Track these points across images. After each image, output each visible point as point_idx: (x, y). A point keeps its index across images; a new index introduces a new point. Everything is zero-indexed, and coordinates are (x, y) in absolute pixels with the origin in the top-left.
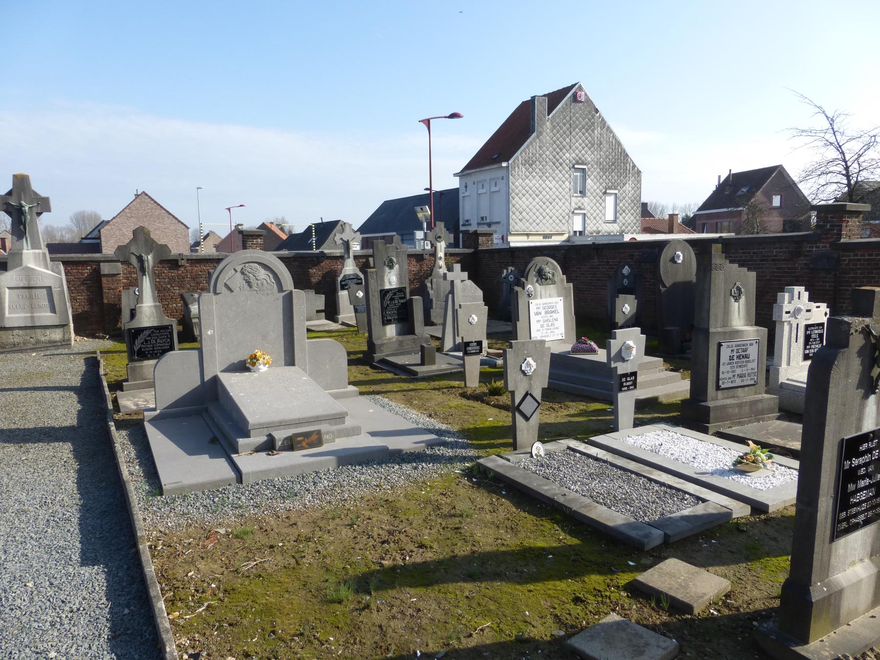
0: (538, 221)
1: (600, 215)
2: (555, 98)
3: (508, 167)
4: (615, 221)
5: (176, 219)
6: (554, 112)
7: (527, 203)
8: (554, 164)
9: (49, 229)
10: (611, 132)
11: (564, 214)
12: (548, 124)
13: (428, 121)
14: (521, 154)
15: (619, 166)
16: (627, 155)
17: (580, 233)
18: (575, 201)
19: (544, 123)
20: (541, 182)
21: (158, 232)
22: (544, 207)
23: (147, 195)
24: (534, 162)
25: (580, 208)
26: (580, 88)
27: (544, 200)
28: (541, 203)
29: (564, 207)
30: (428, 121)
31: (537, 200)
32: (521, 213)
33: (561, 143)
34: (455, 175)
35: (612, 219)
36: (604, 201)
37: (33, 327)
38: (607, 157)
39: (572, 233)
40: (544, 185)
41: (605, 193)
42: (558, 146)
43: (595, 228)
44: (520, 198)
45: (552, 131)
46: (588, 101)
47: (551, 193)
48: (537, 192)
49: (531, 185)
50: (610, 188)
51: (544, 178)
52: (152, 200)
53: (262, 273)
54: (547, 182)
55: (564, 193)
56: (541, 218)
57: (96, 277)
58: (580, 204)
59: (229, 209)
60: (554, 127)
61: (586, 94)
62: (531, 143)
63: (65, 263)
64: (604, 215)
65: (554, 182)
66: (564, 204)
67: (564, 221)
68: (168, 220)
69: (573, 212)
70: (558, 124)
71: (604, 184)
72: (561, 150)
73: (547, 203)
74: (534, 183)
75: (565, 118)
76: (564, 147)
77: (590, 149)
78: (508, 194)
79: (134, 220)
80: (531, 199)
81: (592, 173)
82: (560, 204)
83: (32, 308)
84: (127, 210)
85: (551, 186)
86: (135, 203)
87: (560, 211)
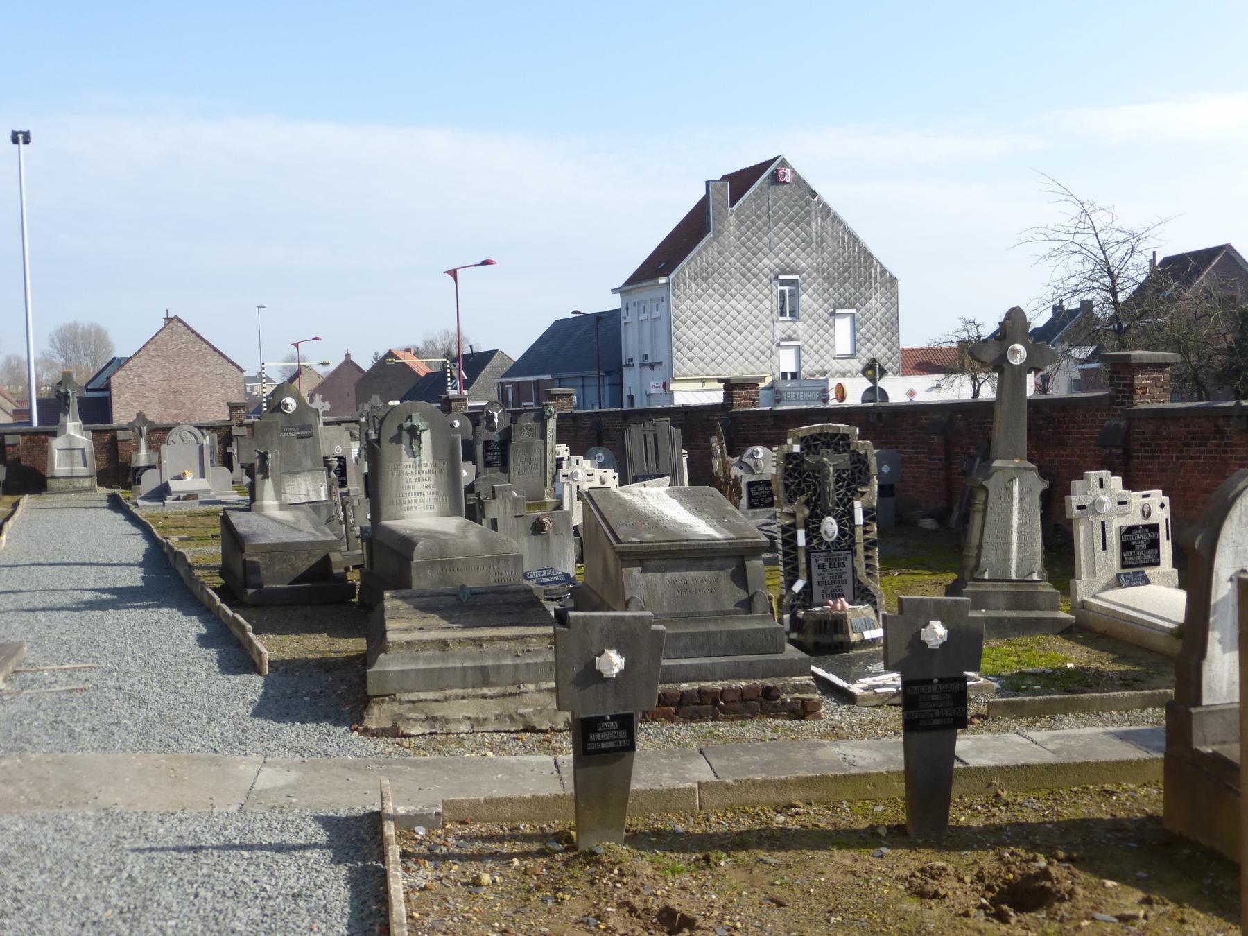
0: (719, 359)
1: (827, 347)
2: (740, 182)
3: (668, 284)
4: (853, 356)
5: (225, 357)
6: (741, 201)
7: (701, 333)
8: (744, 275)
9: (14, 363)
10: (840, 222)
11: (763, 348)
12: (732, 219)
13: (455, 271)
14: (688, 264)
15: (857, 275)
16: (870, 255)
17: (794, 375)
18: (783, 326)
19: (725, 219)
20: (722, 302)
21: (196, 379)
22: (729, 338)
23: (180, 321)
24: (710, 275)
25: (790, 338)
26: (784, 164)
27: (729, 328)
28: (724, 334)
29: (762, 338)
30: (455, 271)
31: (717, 328)
32: (690, 349)
33: (755, 244)
34: (614, 291)
35: (848, 351)
36: (833, 326)
37: (72, 477)
38: (835, 260)
39: (778, 376)
40: (728, 307)
41: (833, 314)
42: (749, 249)
43: (817, 367)
44: (689, 328)
45: (738, 228)
46: (798, 181)
47: (740, 318)
48: (717, 317)
49: (706, 307)
50: (842, 306)
51: (728, 296)
52: (189, 328)
53: (189, 435)
54: (733, 302)
55: (761, 317)
56: (724, 354)
57: (114, 441)
58: (789, 332)
59: (453, 273)
60: (742, 223)
61: (793, 172)
62: (705, 248)
63: (93, 431)
64: (834, 347)
65: (744, 302)
66: (762, 333)
67: (763, 358)
68: (212, 359)
69: (778, 345)
70: (748, 218)
71: (831, 301)
72: (755, 254)
73: (735, 333)
74: (711, 304)
75: (759, 208)
76: (760, 250)
77: (804, 250)
78: (670, 323)
79: (160, 360)
80: (706, 329)
81: (810, 285)
82: (756, 333)
83: (72, 464)
84: (150, 346)
85: (739, 307)
86: (162, 334)
87: (757, 343)
